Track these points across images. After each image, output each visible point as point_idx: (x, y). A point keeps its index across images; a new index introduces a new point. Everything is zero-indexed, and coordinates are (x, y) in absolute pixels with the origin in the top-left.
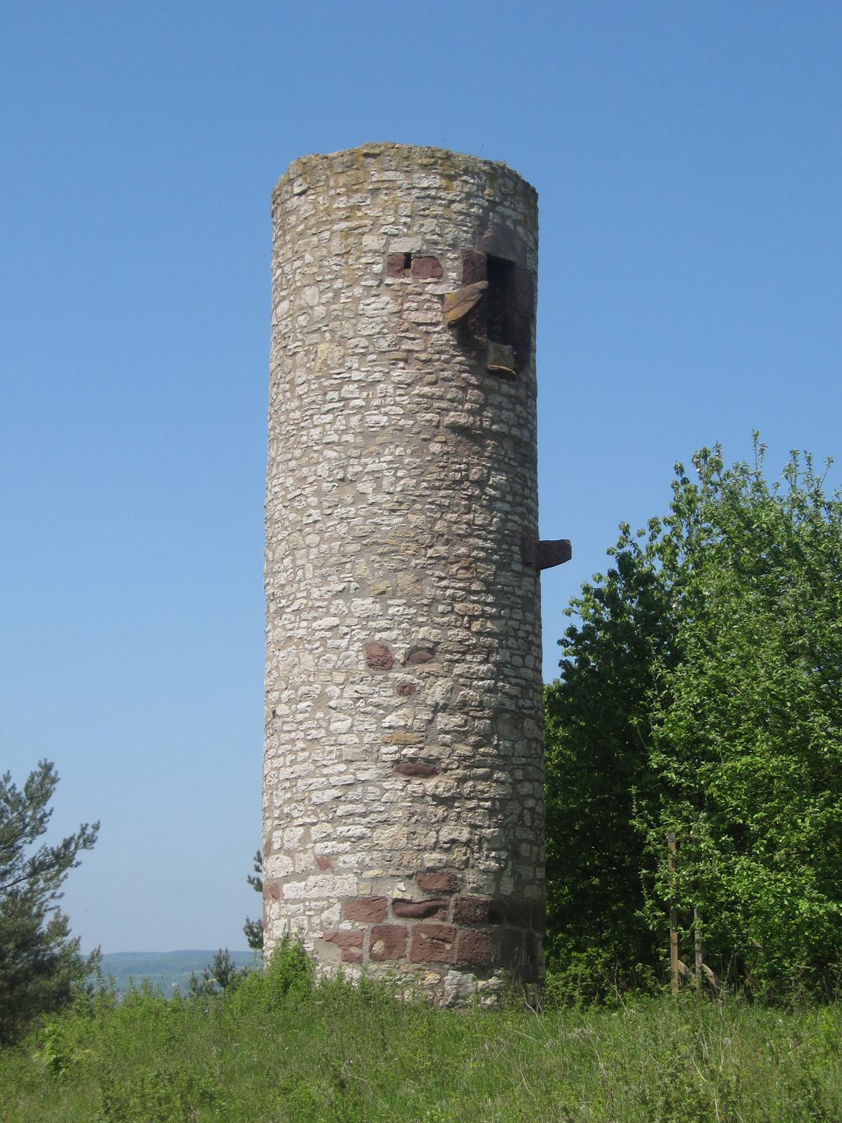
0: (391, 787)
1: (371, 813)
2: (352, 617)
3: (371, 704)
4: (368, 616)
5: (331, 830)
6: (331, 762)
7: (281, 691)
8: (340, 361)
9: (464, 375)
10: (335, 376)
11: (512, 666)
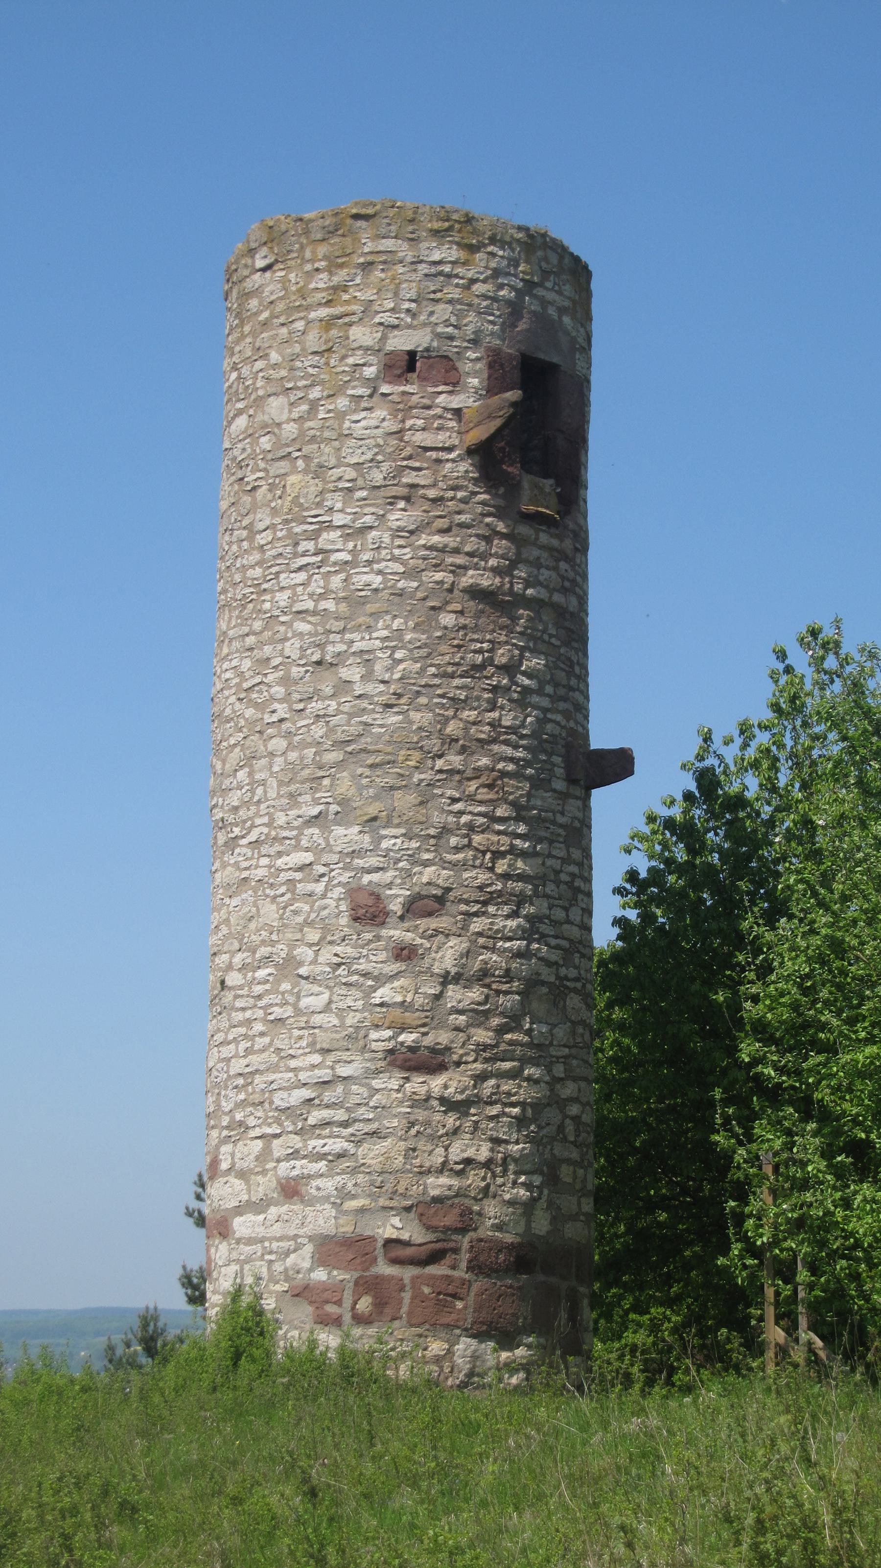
0: (383, 1086)
1: (355, 1121)
2: (331, 851)
3: (356, 972)
4: (354, 852)
5: (300, 1145)
6: (301, 1051)
7: (233, 954)
11: (551, 921)
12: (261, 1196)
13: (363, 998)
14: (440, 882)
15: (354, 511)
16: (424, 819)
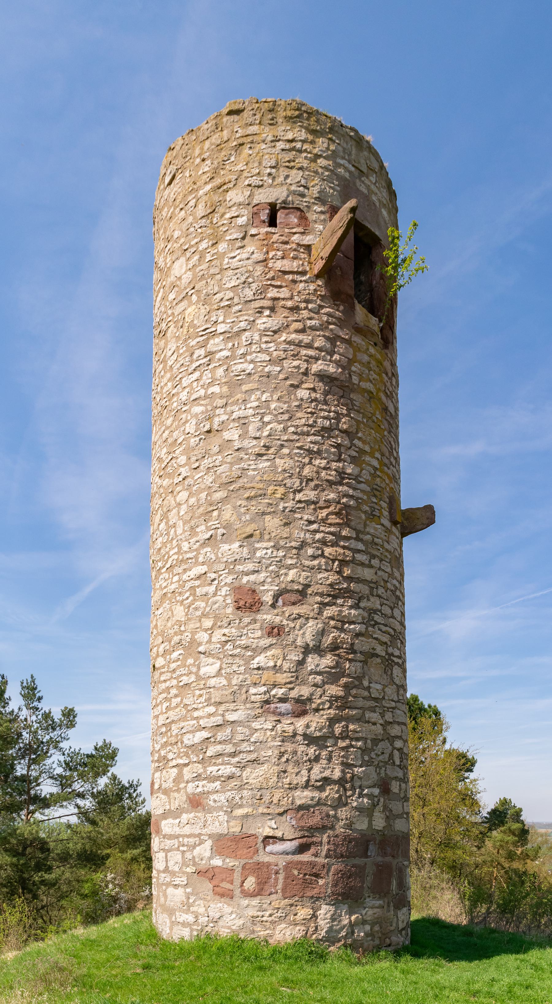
0: (261, 727)
1: (240, 752)
2: (219, 562)
3: (240, 646)
4: (236, 560)
5: (202, 770)
6: (201, 705)
8: (206, 317)
9: (331, 327)
11: (382, 614)
13: (245, 665)
14: (301, 580)
15: (232, 320)
16: (288, 535)
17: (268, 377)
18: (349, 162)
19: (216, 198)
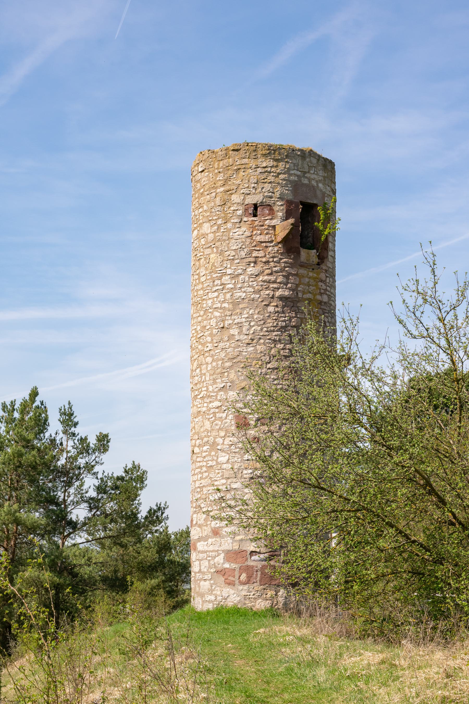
3: (239, 448)
6: (218, 479)
7: (196, 440)
8: (221, 264)
9: (287, 269)
10: (218, 272)
12: (206, 534)
13: (241, 458)
17: (253, 300)
18: (297, 170)
19: (226, 197)
